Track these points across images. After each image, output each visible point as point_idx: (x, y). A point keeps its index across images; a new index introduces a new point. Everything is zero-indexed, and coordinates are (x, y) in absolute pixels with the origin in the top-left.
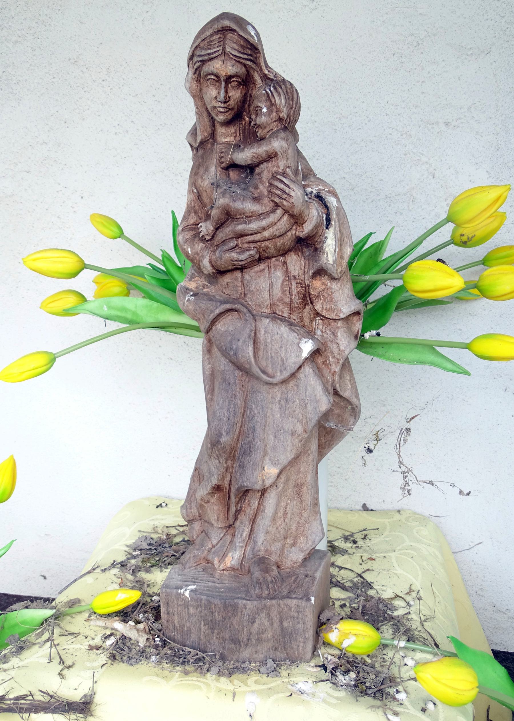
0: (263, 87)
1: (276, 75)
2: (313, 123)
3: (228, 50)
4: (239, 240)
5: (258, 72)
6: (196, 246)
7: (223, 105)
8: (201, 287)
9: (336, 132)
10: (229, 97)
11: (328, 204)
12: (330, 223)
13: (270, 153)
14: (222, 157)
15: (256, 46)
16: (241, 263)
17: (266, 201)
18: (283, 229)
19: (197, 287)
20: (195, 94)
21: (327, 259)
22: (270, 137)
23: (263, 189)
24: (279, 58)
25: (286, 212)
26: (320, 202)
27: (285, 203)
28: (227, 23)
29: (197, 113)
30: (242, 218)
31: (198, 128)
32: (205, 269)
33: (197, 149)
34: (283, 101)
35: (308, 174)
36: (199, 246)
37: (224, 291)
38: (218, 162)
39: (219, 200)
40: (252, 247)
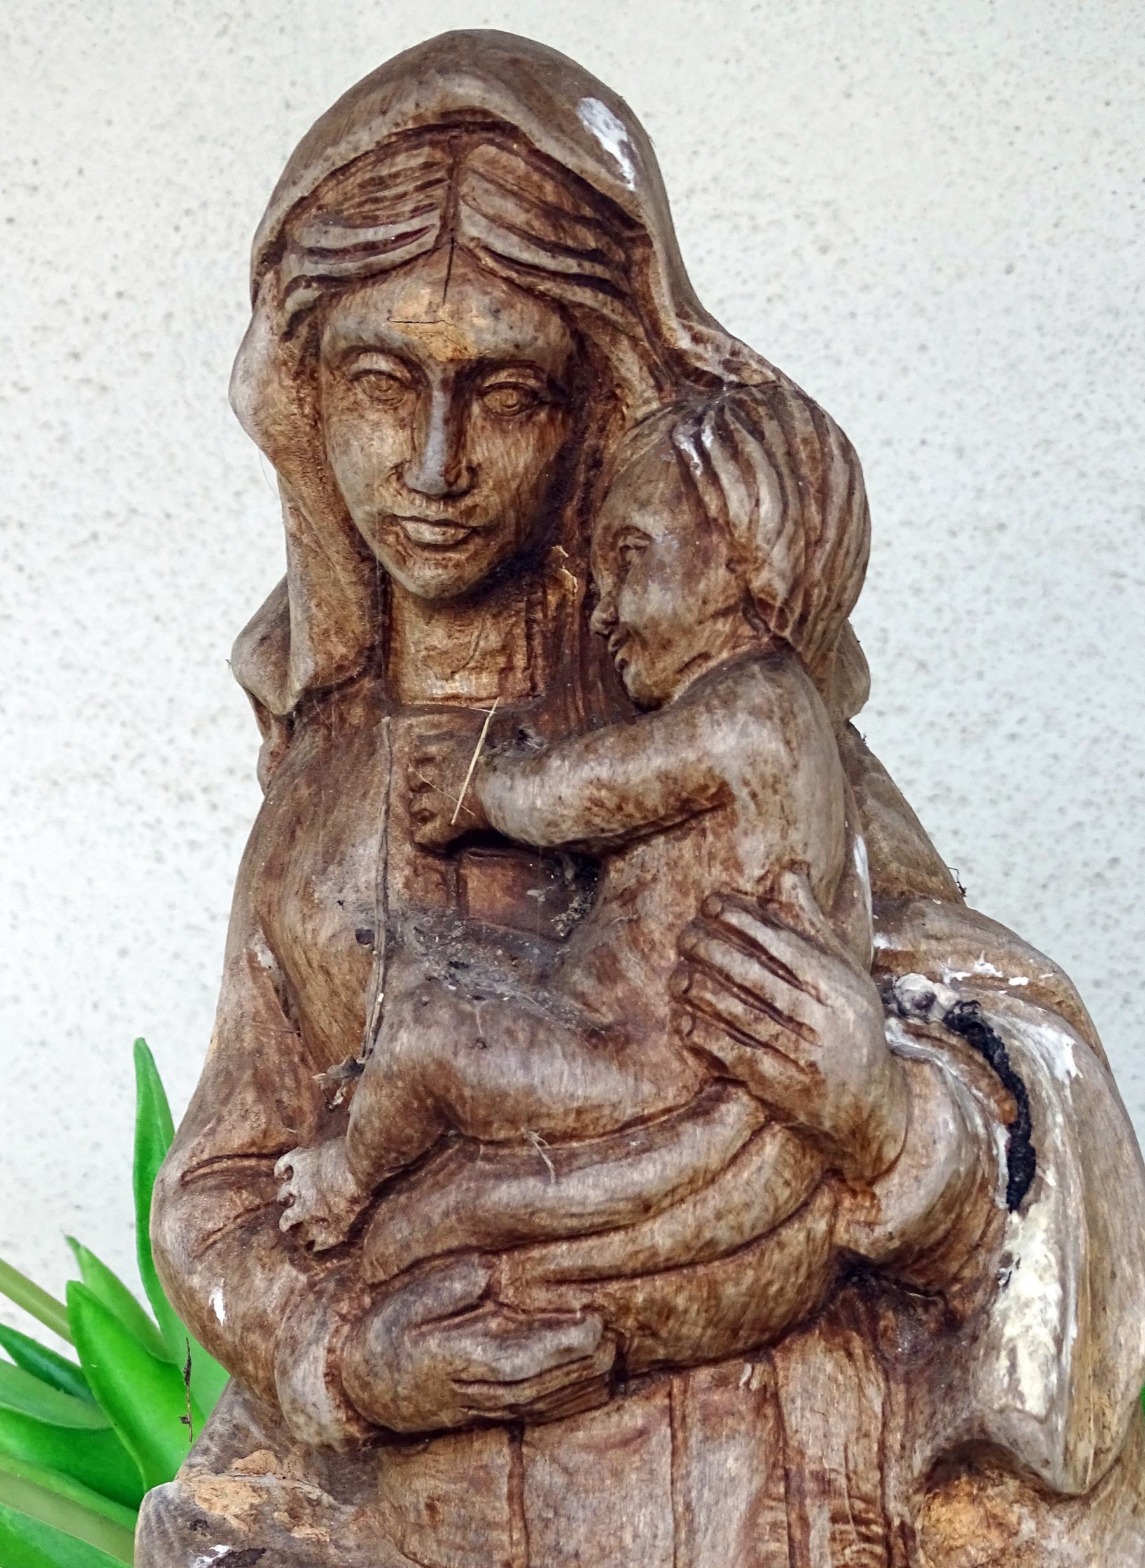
0: (663, 426)
1: (736, 358)
2: (987, 532)
3: (473, 232)
4: (504, 1263)
5: (634, 340)
6: (259, 1279)
7: (434, 511)
8: (281, 1516)
9: (1120, 590)
10: (473, 470)
11: (1024, 1071)
12: (1030, 1176)
13: (691, 786)
14: (424, 787)
15: (629, 208)
16: (508, 1396)
17: (660, 1048)
18: (755, 1212)
19: (256, 1515)
20: (282, 441)
21: (1014, 1388)
22: (689, 700)
23: (647, 982)
24: (748, 272)
25: (774, 1113)
26: (979, 1057)
27: (768, 1065)
28: (469, 91)
29: (294, 538)
30: (524, 1142)
31: (296, 614)
32: (301, 1419)
33: (288, 724)
34: (768, 508)
35: (915, 887)
36: (276, 1283)
37: (413, 1543)
38: (399, 809)
39: (393, 1039)
40: (577, 1305)
